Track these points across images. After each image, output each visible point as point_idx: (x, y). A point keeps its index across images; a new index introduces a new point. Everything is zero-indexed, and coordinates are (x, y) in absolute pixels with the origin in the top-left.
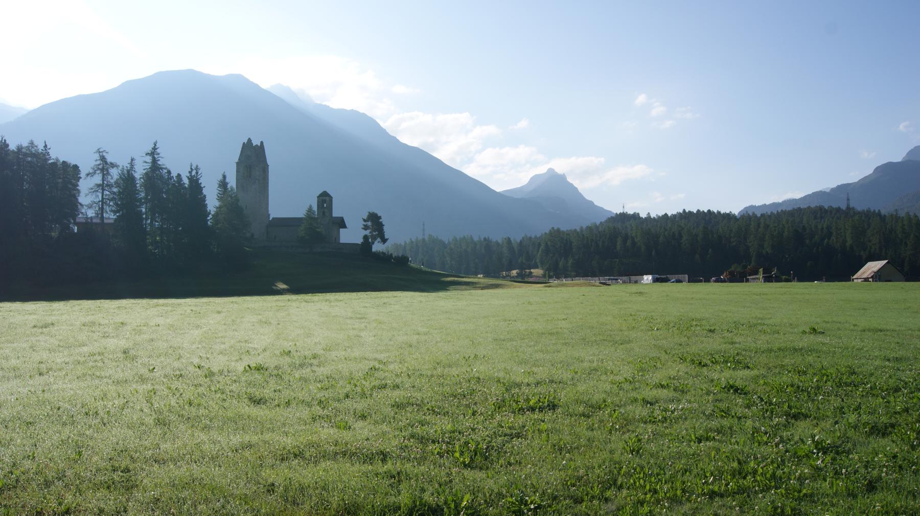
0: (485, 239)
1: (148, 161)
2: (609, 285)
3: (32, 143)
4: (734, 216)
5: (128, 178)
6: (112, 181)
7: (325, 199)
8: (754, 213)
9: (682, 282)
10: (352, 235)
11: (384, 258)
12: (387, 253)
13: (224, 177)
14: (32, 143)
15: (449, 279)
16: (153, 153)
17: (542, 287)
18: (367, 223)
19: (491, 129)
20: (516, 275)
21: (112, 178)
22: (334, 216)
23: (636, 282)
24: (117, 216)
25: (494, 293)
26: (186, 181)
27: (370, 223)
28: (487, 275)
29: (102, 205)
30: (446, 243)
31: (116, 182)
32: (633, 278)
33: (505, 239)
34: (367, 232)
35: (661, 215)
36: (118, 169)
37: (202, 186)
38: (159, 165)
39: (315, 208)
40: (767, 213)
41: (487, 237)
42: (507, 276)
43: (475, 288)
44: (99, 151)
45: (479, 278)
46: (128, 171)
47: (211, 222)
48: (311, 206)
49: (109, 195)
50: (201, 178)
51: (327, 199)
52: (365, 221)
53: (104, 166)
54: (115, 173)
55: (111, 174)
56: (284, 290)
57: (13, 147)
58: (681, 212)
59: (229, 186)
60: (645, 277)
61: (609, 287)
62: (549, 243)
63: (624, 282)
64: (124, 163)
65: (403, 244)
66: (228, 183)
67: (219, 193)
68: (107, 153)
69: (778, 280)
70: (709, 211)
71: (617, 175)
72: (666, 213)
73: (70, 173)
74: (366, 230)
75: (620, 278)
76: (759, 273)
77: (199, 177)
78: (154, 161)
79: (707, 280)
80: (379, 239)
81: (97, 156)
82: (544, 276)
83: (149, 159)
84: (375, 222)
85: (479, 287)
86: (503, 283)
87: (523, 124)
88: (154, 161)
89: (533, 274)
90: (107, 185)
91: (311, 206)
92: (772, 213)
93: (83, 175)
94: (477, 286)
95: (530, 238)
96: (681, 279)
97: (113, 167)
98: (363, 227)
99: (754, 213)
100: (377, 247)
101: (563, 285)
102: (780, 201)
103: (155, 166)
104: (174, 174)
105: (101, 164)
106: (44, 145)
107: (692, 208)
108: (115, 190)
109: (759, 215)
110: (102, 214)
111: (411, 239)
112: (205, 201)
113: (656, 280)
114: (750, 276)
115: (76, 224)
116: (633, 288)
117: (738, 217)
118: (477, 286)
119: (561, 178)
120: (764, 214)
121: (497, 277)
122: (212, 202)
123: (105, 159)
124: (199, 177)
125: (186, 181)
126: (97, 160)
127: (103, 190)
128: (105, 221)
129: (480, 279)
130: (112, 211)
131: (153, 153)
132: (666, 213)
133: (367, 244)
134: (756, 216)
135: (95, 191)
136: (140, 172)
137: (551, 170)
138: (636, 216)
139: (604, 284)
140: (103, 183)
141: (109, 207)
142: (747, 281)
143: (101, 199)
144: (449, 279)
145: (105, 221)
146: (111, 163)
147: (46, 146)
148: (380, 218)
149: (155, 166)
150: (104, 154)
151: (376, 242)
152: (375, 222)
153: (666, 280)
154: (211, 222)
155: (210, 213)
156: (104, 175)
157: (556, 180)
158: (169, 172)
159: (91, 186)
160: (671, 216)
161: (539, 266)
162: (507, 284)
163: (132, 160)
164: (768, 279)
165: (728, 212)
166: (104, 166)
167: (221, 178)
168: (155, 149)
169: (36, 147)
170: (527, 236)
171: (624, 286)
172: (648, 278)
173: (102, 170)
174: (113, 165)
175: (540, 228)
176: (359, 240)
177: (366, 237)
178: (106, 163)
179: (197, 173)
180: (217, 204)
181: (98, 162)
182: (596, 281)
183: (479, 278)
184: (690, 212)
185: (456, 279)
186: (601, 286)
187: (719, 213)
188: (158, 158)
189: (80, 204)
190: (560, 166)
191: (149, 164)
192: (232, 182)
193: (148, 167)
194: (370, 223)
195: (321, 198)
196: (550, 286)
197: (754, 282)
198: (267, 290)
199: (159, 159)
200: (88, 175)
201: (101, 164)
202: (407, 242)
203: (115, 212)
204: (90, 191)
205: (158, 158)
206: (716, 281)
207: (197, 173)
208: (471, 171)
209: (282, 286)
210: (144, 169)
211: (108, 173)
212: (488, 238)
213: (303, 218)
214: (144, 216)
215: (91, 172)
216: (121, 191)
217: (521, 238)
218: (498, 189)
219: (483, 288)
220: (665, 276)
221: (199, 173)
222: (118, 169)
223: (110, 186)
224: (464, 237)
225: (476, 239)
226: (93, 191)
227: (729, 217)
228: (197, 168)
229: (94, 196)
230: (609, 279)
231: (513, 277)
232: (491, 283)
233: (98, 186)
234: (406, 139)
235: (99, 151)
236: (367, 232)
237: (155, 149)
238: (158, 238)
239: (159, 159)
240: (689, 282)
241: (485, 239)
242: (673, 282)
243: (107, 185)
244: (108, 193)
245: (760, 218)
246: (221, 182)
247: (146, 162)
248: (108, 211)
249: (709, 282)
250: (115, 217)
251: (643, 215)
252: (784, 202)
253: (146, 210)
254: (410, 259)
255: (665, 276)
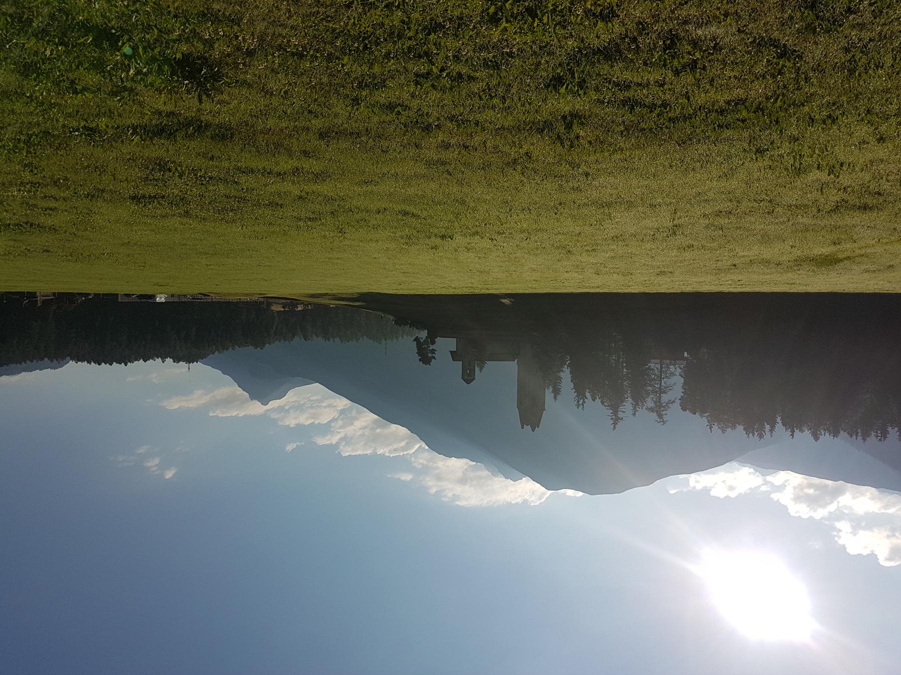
0: (329, 340)
1: (621, 413)
2: (200, 294)
3: (723, 431)
4: (72, 359)
5: (638, 400)
6: (652, 396)
7: (468, 377)
8: (52, 361)
9: (125, 294)
10: (445, 345)
11: (418, 324)
12: (415, 328)
13: (555, 398)
14: (723, 431)
15: (358, 304)
16: (616, 420)
17: (269, 294)
18: (432, 356)
19: (322, 441)
20: (298, 306)
21: (652, 398)
22: (461, 362)
23: (173, 296)
24: (647, 365)
25: (309, 290)
26: (588, 395)
27: (430, 356)
28: (326, 307)
29: (661, 375)
30: (365, 337)
31: (649, 394)
32: (176, 300)
33: (309, 340)
34: (432, 347)
35: (151, 360)
36: (647, 406)
37: (574, 390)
38: (611, 409)
39: (477, 369)
40: (37, 362)
41: (327, 341)
42: (307, 305)
43: (334, 295)
44: (664, 422)
45: (334, 304)
46: (637, 404)
47: (568, 358)
48: (481, 371)
49: (655, 384)
50: (575, 397)
51: (466, 378)
52: (434, 358)
53: (659, 409)
54: (650, 403)
55: (653, 402)
56: (504, 298)
57: (740, 428)
58: (129, 363)
59: (551, 389)
60: (163, 300)
61: (199, 292)
62: (266, 335)
63: (185, 296)
64: (642, 412)
65: (405, 336)
66: (552, 392)
67: (560, 383)
68: (657, 421)
69: (21, 294)
70: (99, 364)
71: (197, 400)
72: (145, 362)
73: (690, 403)
74: (433, 349)
75: (190, 300)
76: (41, 301)
77: (576, 398)
78: (615, 412)
79: (97, 295)
80: (422, 341)
81: (665, 418)
82: (269, 304)
83: (620, 415)
84: (425, 356)
85: (330, 295)
86: (307, 298)
87: (290, 447)
88: (615, 412)
89: (281, 306)
90: (657, 392)
91: (481, 371)
92: (32, 361)
93: (678, 402)
94: (332, 297)
95: (285, 340)
96: (126, 298)
97: (651, 408)
98: (435, 352)
99: (52, 361)
100: (423, 334)
101: (247, 295)
102: (23, 373)
103: (615, 409)
104: (598, 401)
105: (662, 411)
106: (712, 429)
107: (117, 368)
108: (650, 388)
109: (46, 359)
110: (661, 368)
111: (397, 340)
112: (571, 377)
113: (153, 297)
114: (53, 299)
115: (686, 359)
116: (175, 290)
117: (68, 358)
118: (332, 297)
119: (254, 396)
120: (40, 361)
121: (315, 304)
122: (566, 375)
123: (658, 416)
124: (576, 398)
125: (588, 395)
126: (665, 415)
127: (660, 388)
128: (658, 361)
129: (333, 303)
130: (653, 370)
131: (616, 420)
132: (145, 362)
133: (432, 339)
134: (49, 358)
135: (667, 387)
136: (628, 405)
137: (265, 403)
138: (177, 360)
139: (204, 295)
140: (660, 394)
141: (655, 373)
142: (54, 294)
143: (662, 380)
144: (358, 304)
145: (658, 361)
146: (653, 412)
147: (711, 428)
148: (420, 360)
149: (615, 409)
150: (659, 420)
151: (424, 338)
152: (425, 356)
153: (140, 296)
154: (568, 358)
155: (568, 366)
156: (660, 402)
157: (260, 395)
158: (602, 403)
159: (670, 393)
160: (140, 359)
161: (276, 313)
162: (303, 298)
163: (634, 414)
164: (32, 295)
165: (79, 363)
166: (659, 409)
167: (558, 397)
168: (615, 424)
169: (719, 428)
170: (288, 341)
171: (185, 292)
172: (160, 299)
173: (661, 406)
174: (651, 410)
175: (275, 349)
176: (439, 340)
177: (433, 343)
178: (657, 412)
179: (578, 402)
180: (561, 374)
181: (664, 413)
182: (216, 298)
183: (334, 304)
184: (121, 364)
185: (351, 304)
186: (208, 293)
187: (89, 362)
188: (612, 416)
189: (682, 376)
190: (256, 408)
191: (621, 410)
192: (549, 394)
193: (621, 407)
194: (430, 356)
195: (472, 378)
196: (260, 294)
197: (47, 293)
198: (517, 298)
199: (611, 415)
200: (674, 402)
201: (662, 411)
202: (401, 337)
203: (649, 368)
204: (671, 388)
205: (612, 416)
206: (89, 294)
207: (578, 402)
208: (343, 402)
209: (506, 301)
210: (624, 405)
211: (655, 402)
212: (325, 340)
213: (487, 361)
214: (625, 365)
215: (671, 405)
216: (644, 387)
217: (294, 339)
218: (317, 385)
219: (326, 294)
220: (142, 300)
221: (576, 401)
222: (647, 406)
223: (654, 392)
224: (348, 341)
225: (337, 340)
226: (669, 388)
227: (79, 358)
228: (578, 406)
229: (668, 383)
230: (201, 299)
231: (301, 304)
232: (318, 299)
233: (665, 392)
234: (403, 431)
235: (664, 422)
236: (432, 347)
237: (615, 424)
238: (613, 345)
239: (611, 415)
240: (117, 294)
241: (329, 340)
242: (133, 295)
243: (657, 392)
244: (656, 386)
245: (45, 357)
246: (559, 394)
247: (623, 412)
248: (656, 370)
249: (95, 294)
250: (649, 365)
251: (169, 360)
252: (19, 373)
253: (623, 370)
254: (393, 323)
255: (142, 300)
